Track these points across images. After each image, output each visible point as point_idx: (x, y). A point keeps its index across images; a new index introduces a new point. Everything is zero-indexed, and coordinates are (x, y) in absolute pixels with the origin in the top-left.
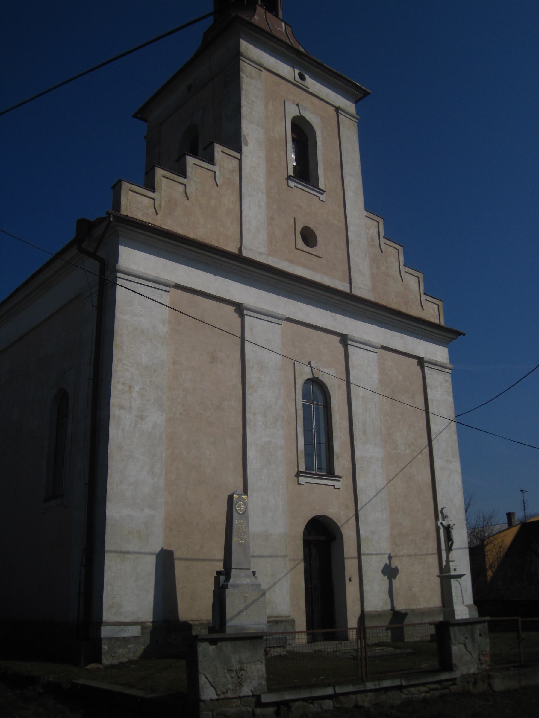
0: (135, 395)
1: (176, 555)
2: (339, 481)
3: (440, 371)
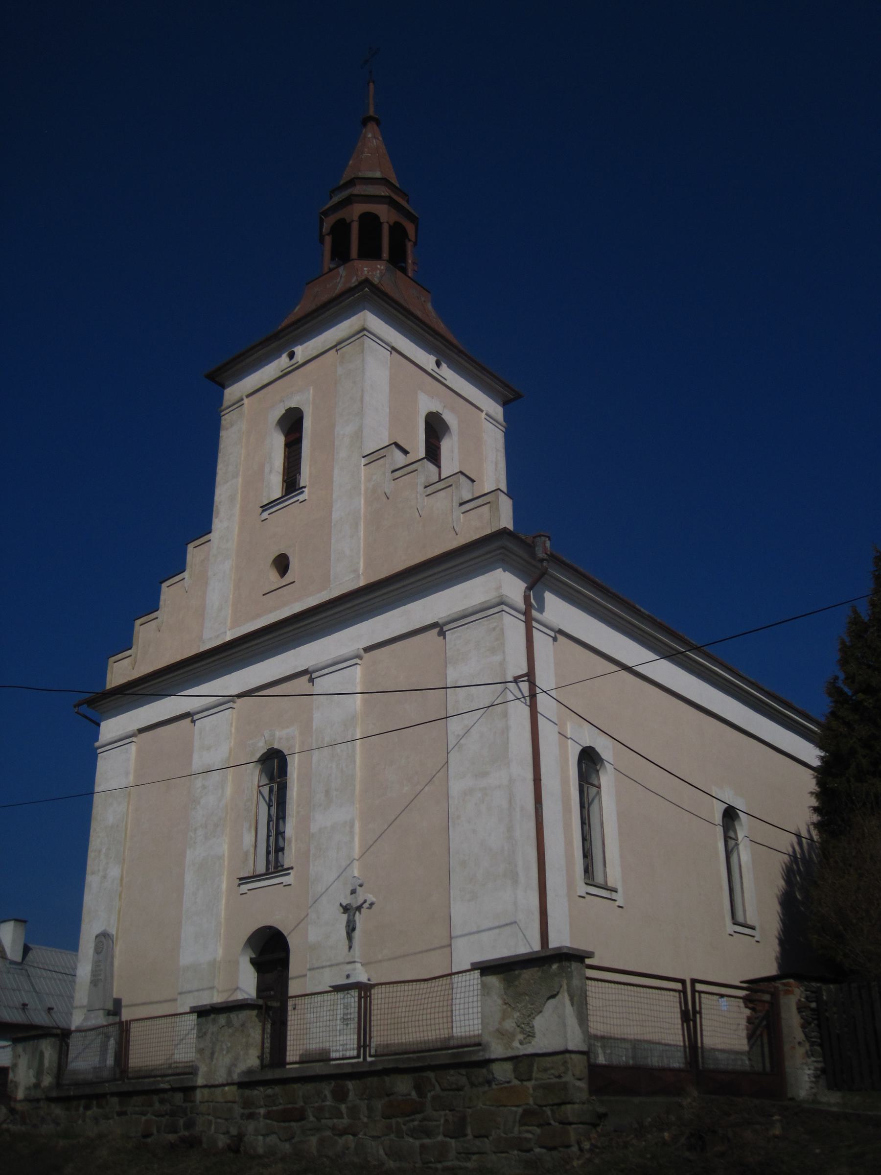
0: (102, 857)
1: (124, 1003)
2: (289, 874)
3: (480, 620)
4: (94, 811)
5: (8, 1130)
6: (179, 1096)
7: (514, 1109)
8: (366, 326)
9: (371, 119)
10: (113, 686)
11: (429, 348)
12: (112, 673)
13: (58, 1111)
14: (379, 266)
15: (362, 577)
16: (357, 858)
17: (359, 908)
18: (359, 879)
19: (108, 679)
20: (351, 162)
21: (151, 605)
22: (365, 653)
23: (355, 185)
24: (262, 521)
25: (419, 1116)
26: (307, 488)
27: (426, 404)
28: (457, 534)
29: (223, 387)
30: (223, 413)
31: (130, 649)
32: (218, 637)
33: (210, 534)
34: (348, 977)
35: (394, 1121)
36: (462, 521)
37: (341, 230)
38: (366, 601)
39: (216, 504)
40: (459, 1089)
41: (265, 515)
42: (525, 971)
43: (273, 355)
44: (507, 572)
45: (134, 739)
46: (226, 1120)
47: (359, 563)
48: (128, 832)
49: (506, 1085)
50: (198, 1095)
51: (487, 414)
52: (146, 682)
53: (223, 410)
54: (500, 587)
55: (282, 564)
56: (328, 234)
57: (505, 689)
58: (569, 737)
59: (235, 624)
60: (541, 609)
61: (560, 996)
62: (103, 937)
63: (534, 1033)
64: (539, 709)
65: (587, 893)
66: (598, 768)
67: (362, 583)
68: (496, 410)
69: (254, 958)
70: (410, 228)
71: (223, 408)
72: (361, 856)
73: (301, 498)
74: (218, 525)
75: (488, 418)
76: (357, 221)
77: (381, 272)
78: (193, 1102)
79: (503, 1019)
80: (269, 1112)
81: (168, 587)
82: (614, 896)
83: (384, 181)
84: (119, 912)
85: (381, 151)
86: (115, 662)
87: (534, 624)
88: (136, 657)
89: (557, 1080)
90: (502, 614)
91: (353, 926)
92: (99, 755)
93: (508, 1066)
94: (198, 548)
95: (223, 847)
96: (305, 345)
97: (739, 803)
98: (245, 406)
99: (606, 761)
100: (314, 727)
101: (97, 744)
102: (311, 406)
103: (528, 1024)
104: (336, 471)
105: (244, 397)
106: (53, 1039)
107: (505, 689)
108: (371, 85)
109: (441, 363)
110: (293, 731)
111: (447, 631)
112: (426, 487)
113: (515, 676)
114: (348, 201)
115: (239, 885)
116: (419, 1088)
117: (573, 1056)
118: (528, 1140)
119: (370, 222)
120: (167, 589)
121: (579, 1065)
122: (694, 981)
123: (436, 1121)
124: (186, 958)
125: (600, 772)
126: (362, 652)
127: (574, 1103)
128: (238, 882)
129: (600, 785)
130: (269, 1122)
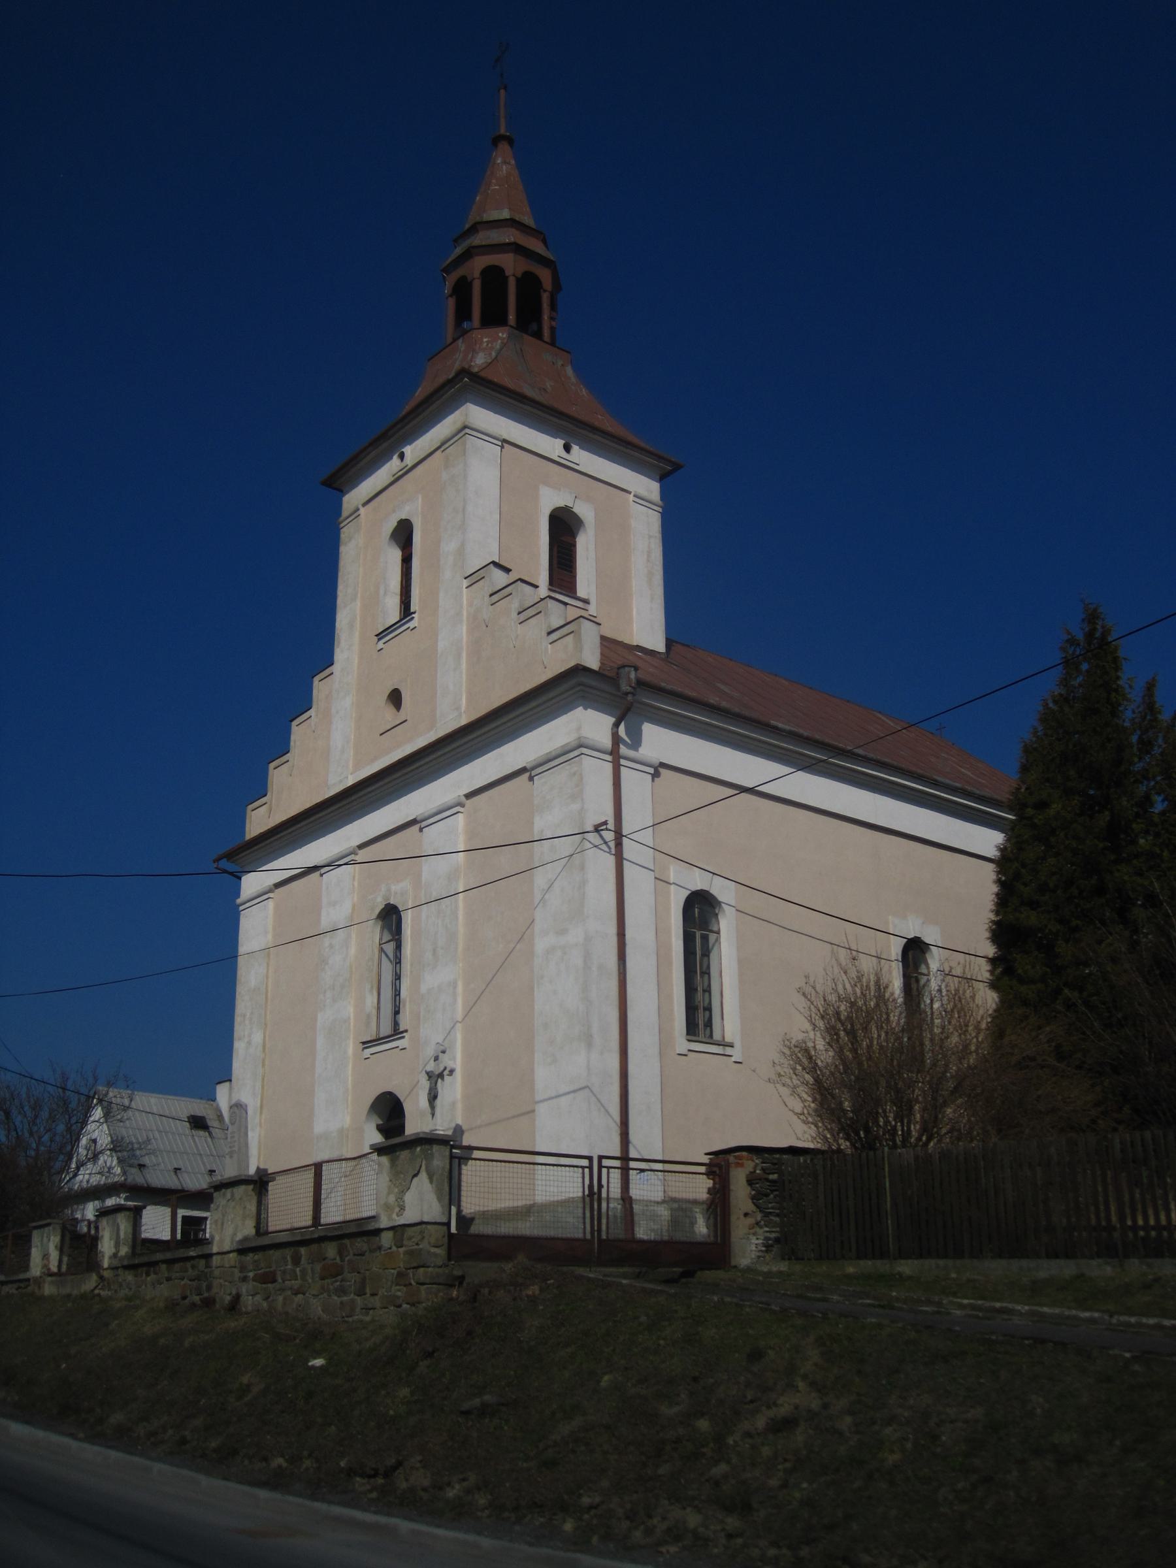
0: (247, 1022)
2: (403, 1037)
4: (239, 973)
5: (99, 1295)
6: (202, 1262)
7: (392, 1271)
8: (467, 423)
10: (252, 836)
11: (553, 431)
12: (251, 822)
13: (129, 1277)
14: (500, 335)
15: (464, 716)
16: (460, 1020)
17: (441, 1076)
18: (442, 1045)
19: (247, 829)
20: (478, 198)
21: (282, 748)
22: (467, 800)
23: (477, 231)
24: (379, 651)
25: (339, 1278)
26: (416, 614)
27: (550, 499)
28: (545, 668)
29: (342, 491)
30: (342, 525)
31: (266, 795)
32: (341, 781)
33: (333, 666)
35: (326, 1281)
36: (549, 652)
37: (462, 289)
39: (337, 632)
40: (362, 1255)
41: (381, 644)
42: (402, 1152)
43: (384, 458)
44: (589, 710)
45: (271, 895)
46: (230, 1282)
47: (461, 699)
48: (269, 994)
49: (389, 1251)
50: (216, 1261)
51: (635, 496)
52: (277, 834)
53: (342, 522)
54: (579, 729)
55: (395, 698)
56: (451, 296)
57: (582, 840)
58: (671, 882)
59: (357, 767)
60: (636, 743)
61: (420, 1175)
62: (236, 1108)
63: (405, 1207)
64: (625, 856)
65: (689, 1050)
66: (717, 912)
67: (464, 721)
68: (650, 488)
69: (382, 1125)
70: (545, 275)
71: (341, 519)
72: (466, 1016)
73: (411, 625)
74: (340, 655)
75: (638, 500)
76: (478, 278)
77: (502, 343)
78: (211, 1267)
79: (389, 1194)
80: (256, 1275)
81: (297, 726)
82: (728, 1051)
83: (512, 223)
84: (263, 1079)
85: (512, 179)
86: (253, 810)
87: (623, 762)
88: (271, 804)
89: (416, 1247)
90: (581, 758)
91: (435, 1093)
92: (242, 912)
93: (390, 1234)
94: (323, 681)
95: (348, 1009)
96: (414, 444)
97: (930, 936)
98: (362, 516)
99: (724, 903)
100: (423, 882)
101: (239, 901)
102: (420, 516)
103: (402, 1199)
104: (441, 595)
105: (360, 506)
106: (128, 1213)
107: (582, 840)
108: (502, 91)
109: (571, 446)
110: (406, 885)
111: (535, 776)
112: (519, 613)
113: (596, 824)
114: (468, 254)
115: (363, 1050)
116: (341, 1252)
117: (429, 1227)
118: (398, 1297)
119: (493, 276)
120: (296, 728)
121: (437, 1233)
122: (601, 1158)
123: (350, 1281)
124: (319, 1128)
125: (719, 917)
126: (463, 799)
127: (428, 1267)
128: (361, 1046)
129: (719, 929)
130: (254, 1283)
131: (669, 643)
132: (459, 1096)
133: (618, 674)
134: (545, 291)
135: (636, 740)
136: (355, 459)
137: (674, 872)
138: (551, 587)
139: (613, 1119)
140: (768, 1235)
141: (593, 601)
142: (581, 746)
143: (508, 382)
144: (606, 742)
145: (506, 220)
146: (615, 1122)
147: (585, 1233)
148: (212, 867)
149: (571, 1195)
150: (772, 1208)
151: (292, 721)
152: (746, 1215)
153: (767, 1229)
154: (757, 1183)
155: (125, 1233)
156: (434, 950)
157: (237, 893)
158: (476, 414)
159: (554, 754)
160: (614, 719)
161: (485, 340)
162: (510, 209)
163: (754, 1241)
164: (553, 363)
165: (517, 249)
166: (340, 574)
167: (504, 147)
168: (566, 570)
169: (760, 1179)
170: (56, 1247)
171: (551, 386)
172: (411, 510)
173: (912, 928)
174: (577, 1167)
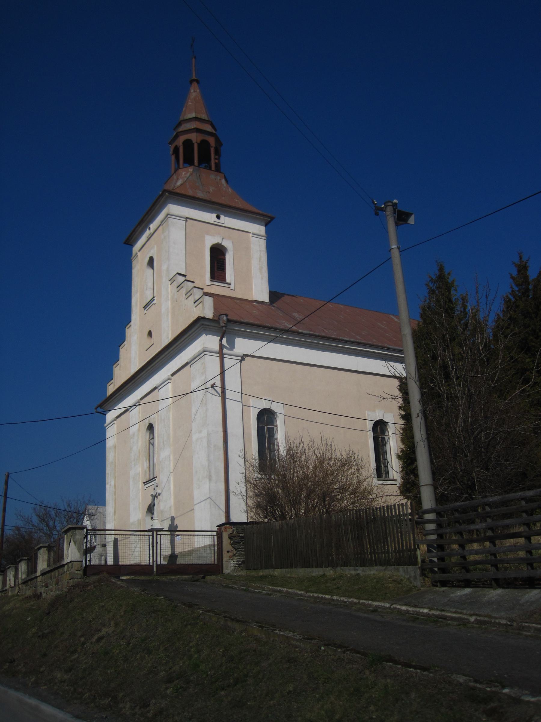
8: (169, 213)
9: (194, 80)
11: (211, 211)
27: (210, 241)
34: (152, 526)
37: (176, 151)
38: (168, 353)
48: (116, 464)
51: (252, 234)
53: (133, 258)
55: (150, 334)
56: (173, 154)
68: (260, 229)
70: (212, 141)
75: (254, 236)
83: (196, 119)
87: (225, 356)
98: (139, 256)
101: (105, 425)
106: (25, 561)
108: (194, 59)
114: (177, 136)
117: (74, 563)
119: (188, 144)
126: (170, 377)
128: (143, 484)
131: (274, 295)
132: (172, 503)
133: (219, 318)
134: (212, 147)
135: (232, 346)
136: (134, 231)
137: (252, 402)
138: (211, 280)
139: (222, 510)
140: (239, 559)
141: (232, 283)
142: (204, 351)
143: (190, 193)
144: (217, 348)
145: (193, 118)
146: (223, 512)
147: (214, 561)
148: (95, 411)
149: (205, 544)
150: (242, 548)
151: (120, 346)
152: (228, 552)
153: (239, 557)
154: (234, 538)
155: (24, 569)
156: (163, 442)
157: (104, 421)
158: (173, 208)
159: (196, 355)
160: (219, 338)
161: (183, 173)
162: (195, 112)
163: (232, 562)
164: (215, 179)
165: (197, 130)
166: (133, 282)
167: (195, 84)
168: (222, 271)
169: (235, 536)
170: (13, 576)
171: (212, 190)
172: (153, 252)
173: (378, 416)
174: (146, 535)
